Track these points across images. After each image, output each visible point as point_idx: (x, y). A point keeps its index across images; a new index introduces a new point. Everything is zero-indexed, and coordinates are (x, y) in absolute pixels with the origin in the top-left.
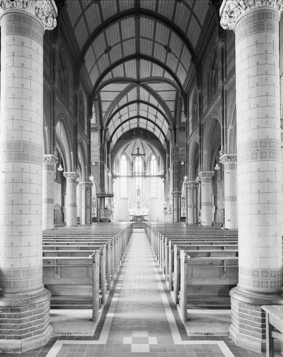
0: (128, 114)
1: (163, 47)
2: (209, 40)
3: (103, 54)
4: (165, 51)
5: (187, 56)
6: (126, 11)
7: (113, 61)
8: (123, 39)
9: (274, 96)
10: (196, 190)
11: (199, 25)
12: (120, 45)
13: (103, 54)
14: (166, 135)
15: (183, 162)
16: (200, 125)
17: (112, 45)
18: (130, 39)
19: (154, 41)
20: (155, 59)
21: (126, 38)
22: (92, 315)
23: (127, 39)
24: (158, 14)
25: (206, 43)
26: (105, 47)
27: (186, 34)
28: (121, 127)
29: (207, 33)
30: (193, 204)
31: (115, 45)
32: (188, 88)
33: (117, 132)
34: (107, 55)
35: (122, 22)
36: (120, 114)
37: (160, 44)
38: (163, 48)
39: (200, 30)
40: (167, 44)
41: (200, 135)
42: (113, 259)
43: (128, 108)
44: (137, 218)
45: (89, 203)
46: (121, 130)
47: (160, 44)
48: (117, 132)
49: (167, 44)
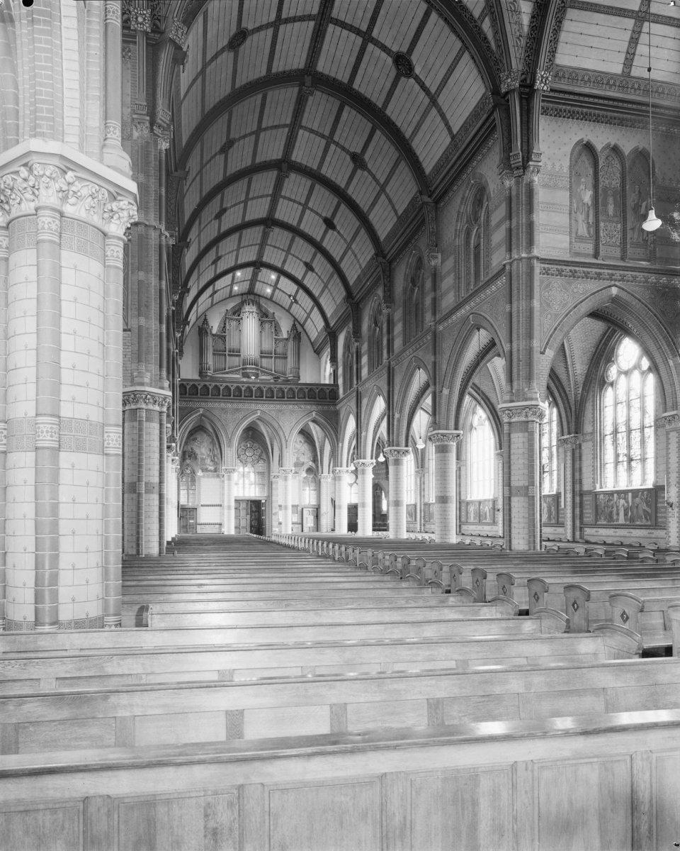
0: (242, 205)
2: (454, 179)
4: (352, 166)
6: (284, 72)
7: (232, 169)
8: (284, 16)
10: (510, 486)
13: (216, 155)
15: (652, 214)
18: (302, 19)
20: (324, 176)
23: (302, 19)
26: (224, 140)
28: (211, 287)
29: (439, 184)
30: (139, 495)
33: (201, 299)
35: (270, 94)
37: (343, 149)
38: (348, 158)
39: (449, 140)
40: (359, 151)
43: (237, 259)
44: (269, 297)
45: (157, 474)
47: (343, 149)
48: (207, 136)
49: (359, 151)
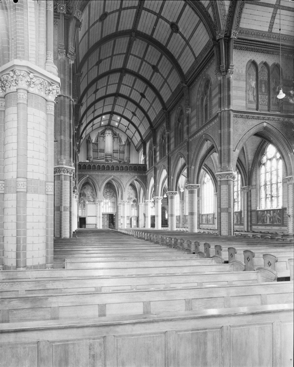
1: (139, 94)
3: (94, 66)
5: (148, 125)
9: (96, 224)
11: (194, 55)
12: (110, 58)
13: (94, 66)
14: (142, 135)
15: (281, 91)
16: (168, 157)
17: (109, 11)
19: (143, 59)
21: (126, 6)
22: (290, 12)
24: (153, 38)
25: (201, 68)
27: (207, 9)
31: (106, 58)
32: (208, 57)
33: (87, 128)
34: (101, 23)
35: (117, 40)
36: (94, 108)
37: (149, 63)
39: (194, 60)
40: (155, 64)
41: (168, 164)
42: (15, 280)
46: (91, 127)
